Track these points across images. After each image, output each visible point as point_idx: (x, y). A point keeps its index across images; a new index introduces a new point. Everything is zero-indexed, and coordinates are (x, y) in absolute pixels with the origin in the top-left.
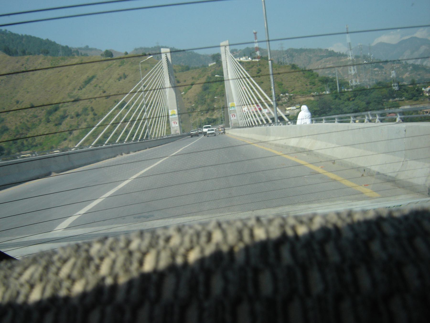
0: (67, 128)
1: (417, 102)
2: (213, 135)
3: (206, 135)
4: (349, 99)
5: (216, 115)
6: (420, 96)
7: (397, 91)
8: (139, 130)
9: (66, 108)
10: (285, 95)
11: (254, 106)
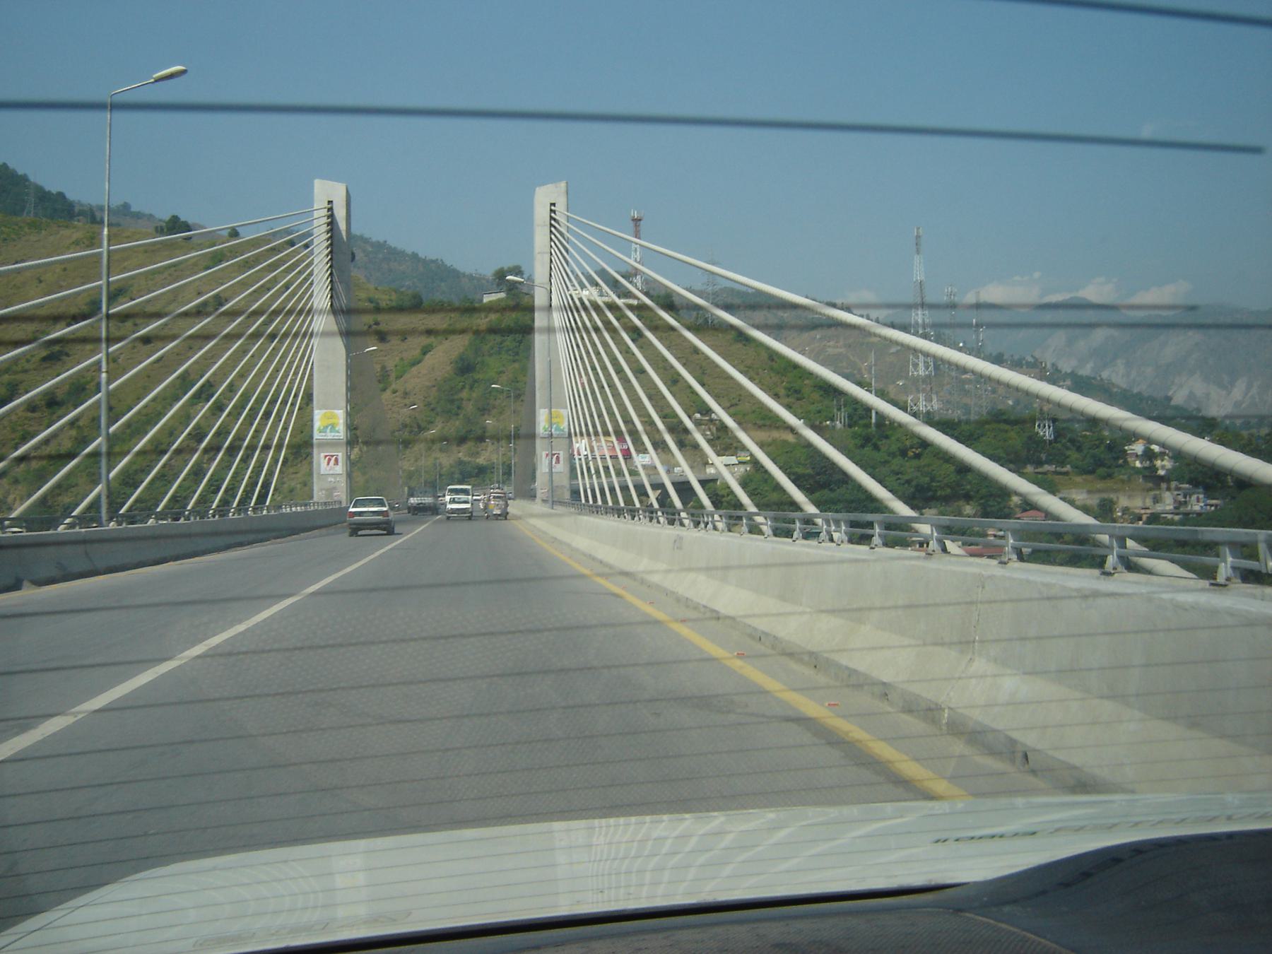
0: (14, 439)
1: (1109, 483)
2: (465, 515)
3: (360, 533)
4: (903, 453)
5: (489, 455)
6: (1117, 467)
7: (1050, 442)
8: (236, 473)
9: (19, 377)
10: (707, 418)
11: (609, 439)
